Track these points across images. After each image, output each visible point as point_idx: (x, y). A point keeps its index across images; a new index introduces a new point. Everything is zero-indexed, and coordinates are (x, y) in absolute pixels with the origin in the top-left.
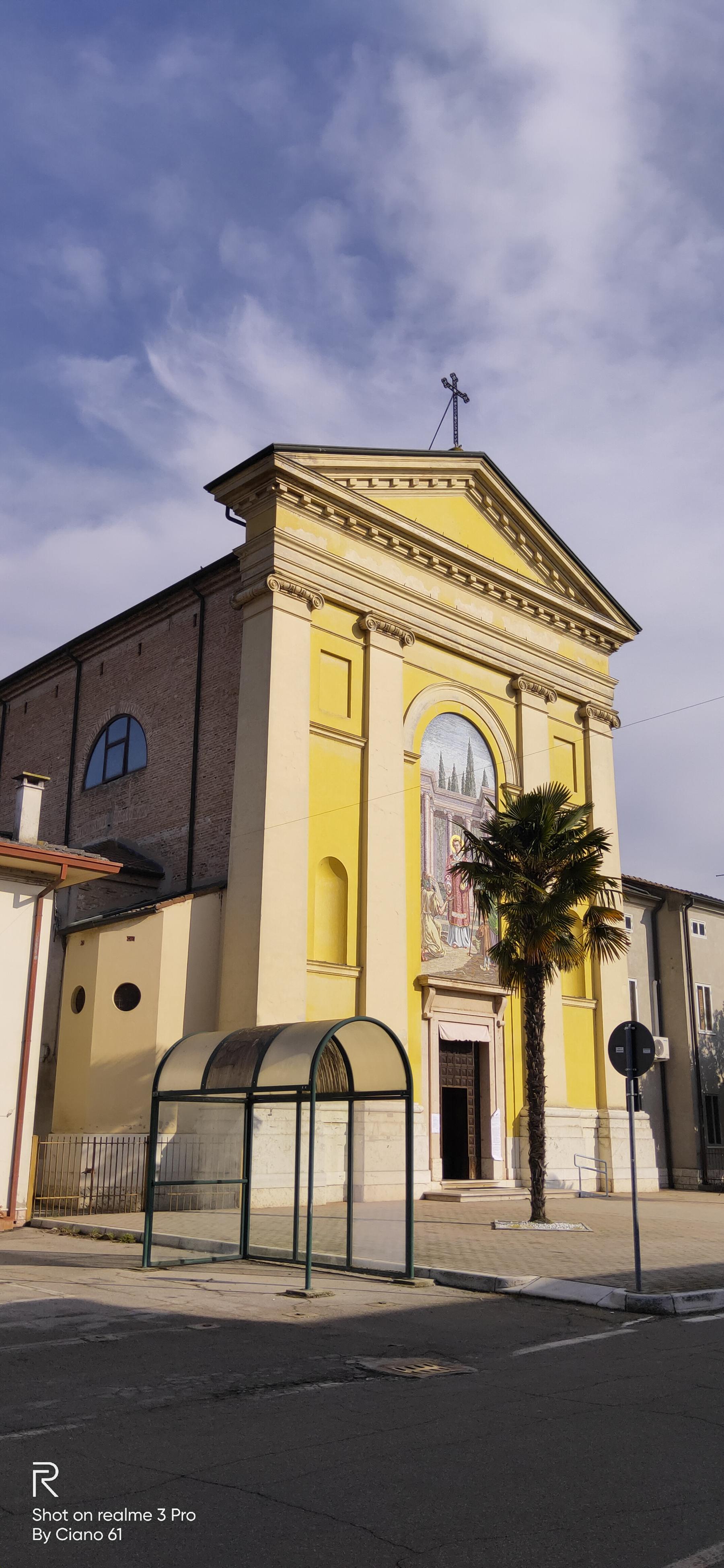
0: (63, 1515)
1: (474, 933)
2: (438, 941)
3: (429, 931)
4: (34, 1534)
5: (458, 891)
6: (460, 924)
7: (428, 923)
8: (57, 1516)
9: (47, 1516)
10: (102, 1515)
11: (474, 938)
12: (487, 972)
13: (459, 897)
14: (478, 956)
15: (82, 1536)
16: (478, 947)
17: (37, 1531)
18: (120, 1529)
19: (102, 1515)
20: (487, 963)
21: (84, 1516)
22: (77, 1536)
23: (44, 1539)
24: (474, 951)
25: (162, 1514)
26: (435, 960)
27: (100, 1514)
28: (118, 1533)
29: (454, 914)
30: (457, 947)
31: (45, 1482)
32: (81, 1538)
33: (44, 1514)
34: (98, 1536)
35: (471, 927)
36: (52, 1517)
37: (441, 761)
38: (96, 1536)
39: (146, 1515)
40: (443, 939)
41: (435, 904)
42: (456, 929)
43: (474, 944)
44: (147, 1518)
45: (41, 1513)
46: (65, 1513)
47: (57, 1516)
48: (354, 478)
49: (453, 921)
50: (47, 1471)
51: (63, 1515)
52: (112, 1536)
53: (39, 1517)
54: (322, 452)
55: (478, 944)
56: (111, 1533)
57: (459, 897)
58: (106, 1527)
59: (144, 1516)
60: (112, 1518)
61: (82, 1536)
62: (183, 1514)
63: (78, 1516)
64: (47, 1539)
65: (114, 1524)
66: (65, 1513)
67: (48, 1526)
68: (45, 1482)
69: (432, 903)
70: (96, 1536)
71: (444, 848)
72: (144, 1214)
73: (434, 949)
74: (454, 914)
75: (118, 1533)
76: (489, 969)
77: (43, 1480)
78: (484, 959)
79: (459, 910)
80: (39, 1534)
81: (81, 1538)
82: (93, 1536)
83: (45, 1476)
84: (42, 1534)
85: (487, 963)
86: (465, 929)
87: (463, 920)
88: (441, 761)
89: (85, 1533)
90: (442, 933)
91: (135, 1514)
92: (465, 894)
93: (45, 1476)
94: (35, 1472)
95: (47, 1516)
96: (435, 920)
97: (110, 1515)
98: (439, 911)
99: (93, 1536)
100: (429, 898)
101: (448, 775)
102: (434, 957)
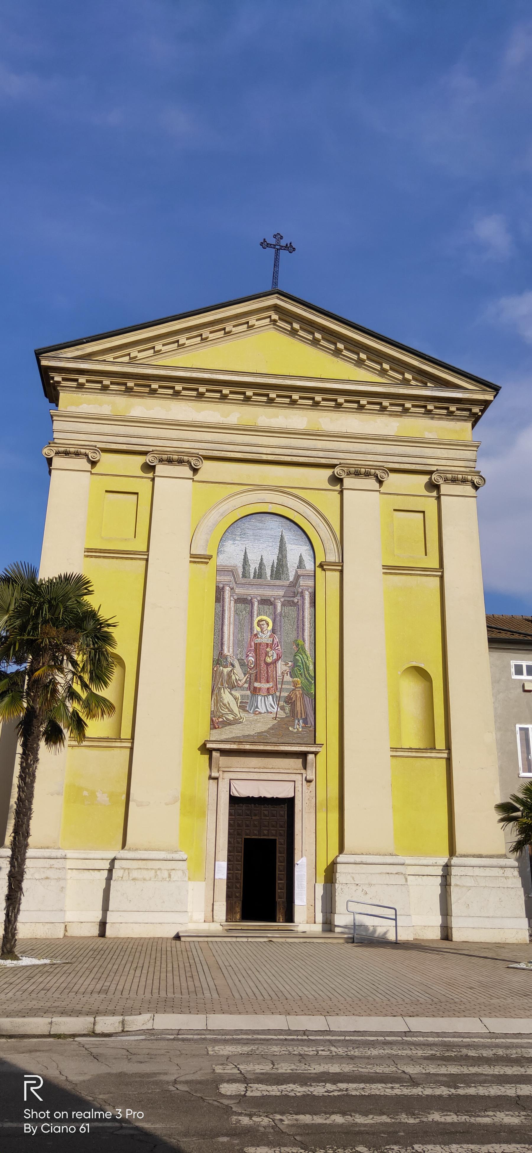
1: (283, 699)
2: (236, 710)
3: (225, 702)
4: (25, 1128)
8: (42, 1115)
9: (35, 1114)
10: (75, 1114)
11: (282, 703)
12: (298, 732)
16: (287, 711)
17: (27, 1126)
19: (75, 1114)
22: (57, 1129)
25: (119, 1113)
26: (230, 727)
27: (73, 1113)
29: (256, 685)
30: (260, 713)
32: (59, 1131)
33: (32, 1113)
35: (278, 694)
36: (38, 1115)
38: (70, 1129)
41: (233, 677)
42: (259, 698)
43: (283, 708)
45: (30, 1113)
46: (48, 1112)
47: (42, 1115)
51: (46, 1114)
52: (83, 1130)
53: (28, 1116)
56: (82, 1127)
59: (106, 1115)
60: (83, 1116)
61: (60, 1129)
62: (134, 1113)
63: (57, 1115)
64: (35, 1132)
66: (48, 1112)
71: (247, 629)
73: (231, 717)
74: (256, 685)
80: (29, 1128)
81: (59, 1131)
84: (31, 1128)
86: (271, 697)
87: (268, 689)
91: (99, 1113)
95: (35, 1114)
96: (233, 692)
97: (80, 1114)
101: (253, 566)
102: (230, 724)
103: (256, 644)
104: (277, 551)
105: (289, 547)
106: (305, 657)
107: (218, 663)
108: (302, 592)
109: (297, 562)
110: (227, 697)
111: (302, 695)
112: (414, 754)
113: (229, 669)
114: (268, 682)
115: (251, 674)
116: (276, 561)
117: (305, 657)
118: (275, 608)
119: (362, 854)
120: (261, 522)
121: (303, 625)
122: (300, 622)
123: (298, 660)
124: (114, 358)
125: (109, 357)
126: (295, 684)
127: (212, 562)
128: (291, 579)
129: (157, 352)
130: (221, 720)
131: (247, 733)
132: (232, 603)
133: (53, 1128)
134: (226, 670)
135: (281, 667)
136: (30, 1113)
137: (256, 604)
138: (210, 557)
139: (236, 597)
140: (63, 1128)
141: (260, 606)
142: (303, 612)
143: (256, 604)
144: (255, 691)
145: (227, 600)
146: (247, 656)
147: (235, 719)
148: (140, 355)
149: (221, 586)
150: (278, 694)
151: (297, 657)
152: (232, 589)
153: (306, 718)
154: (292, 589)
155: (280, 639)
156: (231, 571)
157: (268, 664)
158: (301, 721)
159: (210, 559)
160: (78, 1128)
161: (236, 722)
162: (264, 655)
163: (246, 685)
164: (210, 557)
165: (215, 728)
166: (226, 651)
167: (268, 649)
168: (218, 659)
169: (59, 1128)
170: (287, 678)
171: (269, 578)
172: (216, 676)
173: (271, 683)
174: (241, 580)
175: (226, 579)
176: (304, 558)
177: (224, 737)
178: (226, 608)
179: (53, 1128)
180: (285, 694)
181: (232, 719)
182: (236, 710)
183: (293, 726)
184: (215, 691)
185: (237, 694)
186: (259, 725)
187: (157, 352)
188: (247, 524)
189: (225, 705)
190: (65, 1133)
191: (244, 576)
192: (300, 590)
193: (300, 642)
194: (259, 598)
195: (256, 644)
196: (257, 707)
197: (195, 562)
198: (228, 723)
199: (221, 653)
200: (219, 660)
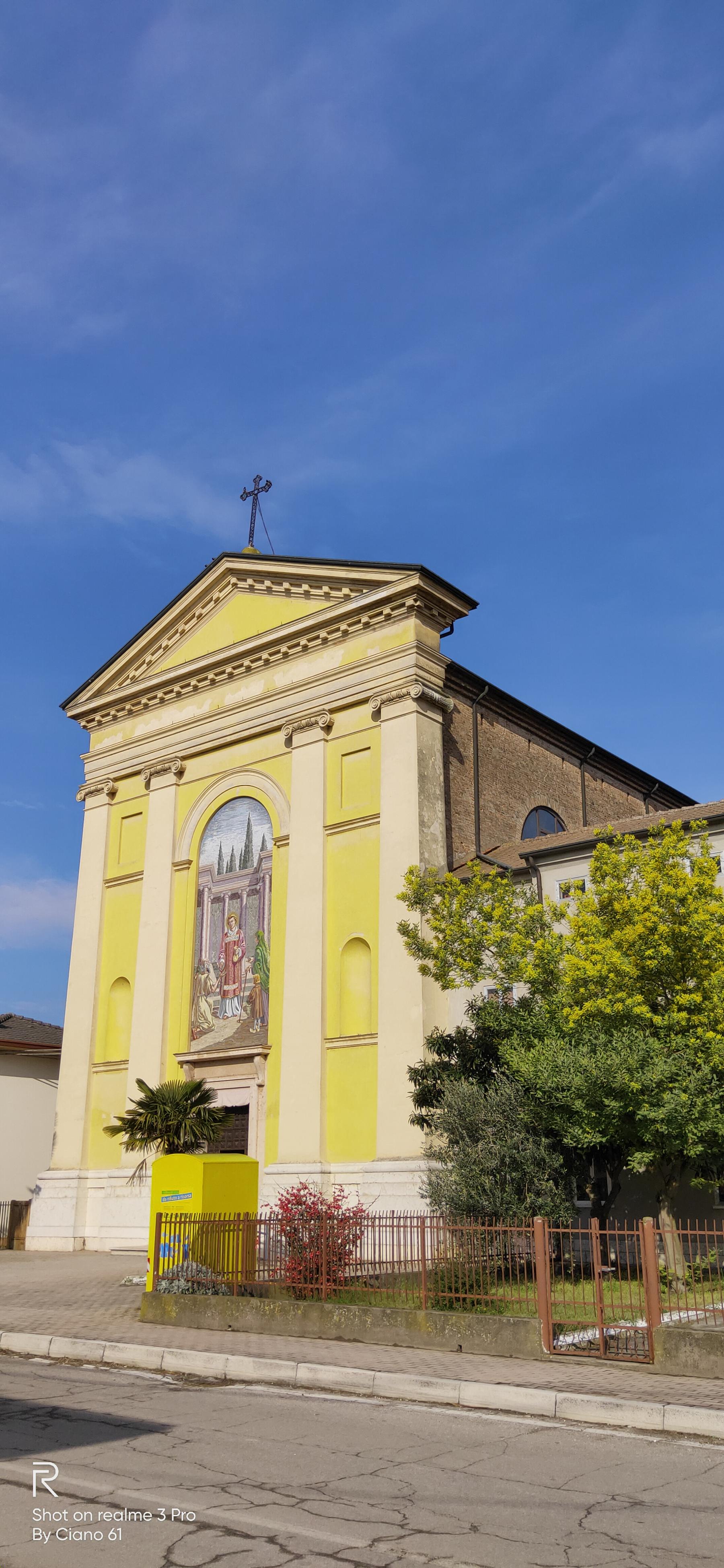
0: (63, 1515)
1: (245, 999)
2: (209, 1017)
3: (202, 1010)
4: (34, 1534)
5: (231, 964)
6: (231, 995)
7: (201, 1004)
8: (57, 1516)
9: (47, 1515)
10: (102, 1515)
11: (245, 1004)
12: (257, 1033)
13: (231, 969)
14: (247, 1021)
15: (83, 1535)
16: (249, 1012)
17: (37, 1531)
18: (120, 1529)
19: (102, 1515)
20: (257, 1025)
21: (84, 1516)
22: (78, 1536)
23: (44, 1539)
24: (245, 1016)
25: (162, 1514)
26: (205, 1036)
27: (100, 1514)
28: (118, 1533)
29: (226, 988)
30: (228, 1017)
31: (46, 1482)
32: (81, 1538)
33: (44, 1514)
34: (98, 1536)
35: (242, 994)
36: (52, 1517)
37: (220, 851)
38: (96, 1536)
39: (146, 1515)
40: (214, 1014)
41: (209, 984)
42: (228, 1001)
43: (245, 1010)
44: (146, 1518)
45: (41, 1513)
46: (65, 1513)
47: (57, 1516)
48: (132, 673)
49: (224, 994)
50: (47, 1471)
51: (63, 1515)
52: (112, 1536)
53: (39, 1517)
54: (93, 681)
55: (249, 1009)
56: (111, 1533)
57: (231, 969)
58: (105, 1527)
59: (144, 1516)
60: (113, 1519)
61: (83, 1535)
62: (183, 1514)
63: (78, 1516)
64: (47, 1539)
65: (113, 1524)
66: (65, 1513)
67: (46, 1525)
68: (46, 1482)
69: (206, 983)
70: (96, 1536)
71: (220, 930)
72: (71, 1250)
73: (205, 1026)
74: (226, 988)
75: (118, 1533)
76: (258, 1030)
77: (43, 1480)
78: (254, 1022)
79: (231, 982)
80: (39, 1534)
81: (81, 1538)
82: (93, 1536)
83: (45, 1475)
84: (42, 1533)
85: (257, 1025)
86: (236, 998)
87: (234, 990)
88: (220, 851)
89: (85, 1533)
90: (214, 1009)
91: (135, 1514)
92: (237, 965)
93: (45, 1475)
94: (35, 1472)
95: (47, 1515)
96: (208, 999)
97: (110, 1515)
98: (212, 989)
99: (93, 1536)
100: (203, 981)
101: (226, 859)
102: (205, 1033)
103: (226, 944)
104: (245, 836)
105: (254, 829)
106: (264, 949)
107: (198, 972)
108: (263, 877)
109: (260, 844)
110: (203, 1006)
111: (261, 991)
112: (349, 1043)
113: (206, 975)
114: (234, 983)
115: (221, 977)
116: (244, 849)
117: (264, 949)
118: (242, 901)
119: (290, 1163)
120: (233, 809)
121: (264, 914)
122: (261, 910)
123: (258, 954)
124: (120, 685)
125: (115, 686)
126: (255, 980)
127: (193, 866)
128: (255, 865)
129: (150, 663)
130: (198, 1030)
131: (217, 1041)
132: (210, 903)
133: (72, 1534)
134: (203, 977)
135: (246, 964)
136: (41, 1513)
137: (227, 900)
138: (190, 862)
139: (212, 897)
140: (85, 1533)
141: (230, 902)
142: (264, 898)
143: (227, 900)
144: (224, 994)
145: (206, 902)
146: (220, 958)
147: (210, 1028)
148: (138, 673)
149: (201, 888)
150: (242, 994)
151: (258, 951)
152: (210, 889)
153: (263, 1017)
154: (255, 876)
155: (245, 934)
156: (208, 871)
157: (234, 964)
158: (259, 1021)
159: (190, 864)
160: (106, 1535)
161: (210, 1030)
162: (232, 954)
163: (218, 990)
164: (190, 862)
165: (194, 1039)
166: (203, 958)
167: (235, 948)
168: (198, 967)
169: (81, 1533)
170: (250, 975)
171: (238, 869)
172: (195, 982)
173: (237, 984)
174: (217, 877)
175: (205, 879)
176: (266, 838)
177: (200, 1048)
178: (205, 911)
179: (72, 1534)
180: (247, 993)
181: (207, 1028)
182: (209, 1017)
183: (253, 1027)
184: (194, 1001)
185: (211, 1000)
186: (227, 1030)
187: (150, 663)
188: (221, 816)
189: (202, 1014)
190: (88, 1541)
191: (219, 873)
192: (262, 875)
193: (261, 934)
194: (229, 894)
195: (226, 944)
196: (226, 1012)
197: (179, 870)
198: (203, 1033)
199: (200, 960)
200: (198, 968)
